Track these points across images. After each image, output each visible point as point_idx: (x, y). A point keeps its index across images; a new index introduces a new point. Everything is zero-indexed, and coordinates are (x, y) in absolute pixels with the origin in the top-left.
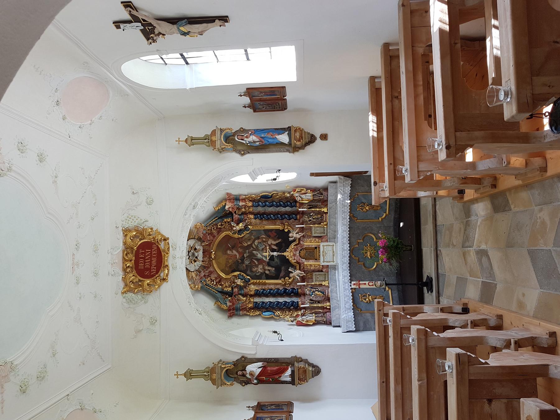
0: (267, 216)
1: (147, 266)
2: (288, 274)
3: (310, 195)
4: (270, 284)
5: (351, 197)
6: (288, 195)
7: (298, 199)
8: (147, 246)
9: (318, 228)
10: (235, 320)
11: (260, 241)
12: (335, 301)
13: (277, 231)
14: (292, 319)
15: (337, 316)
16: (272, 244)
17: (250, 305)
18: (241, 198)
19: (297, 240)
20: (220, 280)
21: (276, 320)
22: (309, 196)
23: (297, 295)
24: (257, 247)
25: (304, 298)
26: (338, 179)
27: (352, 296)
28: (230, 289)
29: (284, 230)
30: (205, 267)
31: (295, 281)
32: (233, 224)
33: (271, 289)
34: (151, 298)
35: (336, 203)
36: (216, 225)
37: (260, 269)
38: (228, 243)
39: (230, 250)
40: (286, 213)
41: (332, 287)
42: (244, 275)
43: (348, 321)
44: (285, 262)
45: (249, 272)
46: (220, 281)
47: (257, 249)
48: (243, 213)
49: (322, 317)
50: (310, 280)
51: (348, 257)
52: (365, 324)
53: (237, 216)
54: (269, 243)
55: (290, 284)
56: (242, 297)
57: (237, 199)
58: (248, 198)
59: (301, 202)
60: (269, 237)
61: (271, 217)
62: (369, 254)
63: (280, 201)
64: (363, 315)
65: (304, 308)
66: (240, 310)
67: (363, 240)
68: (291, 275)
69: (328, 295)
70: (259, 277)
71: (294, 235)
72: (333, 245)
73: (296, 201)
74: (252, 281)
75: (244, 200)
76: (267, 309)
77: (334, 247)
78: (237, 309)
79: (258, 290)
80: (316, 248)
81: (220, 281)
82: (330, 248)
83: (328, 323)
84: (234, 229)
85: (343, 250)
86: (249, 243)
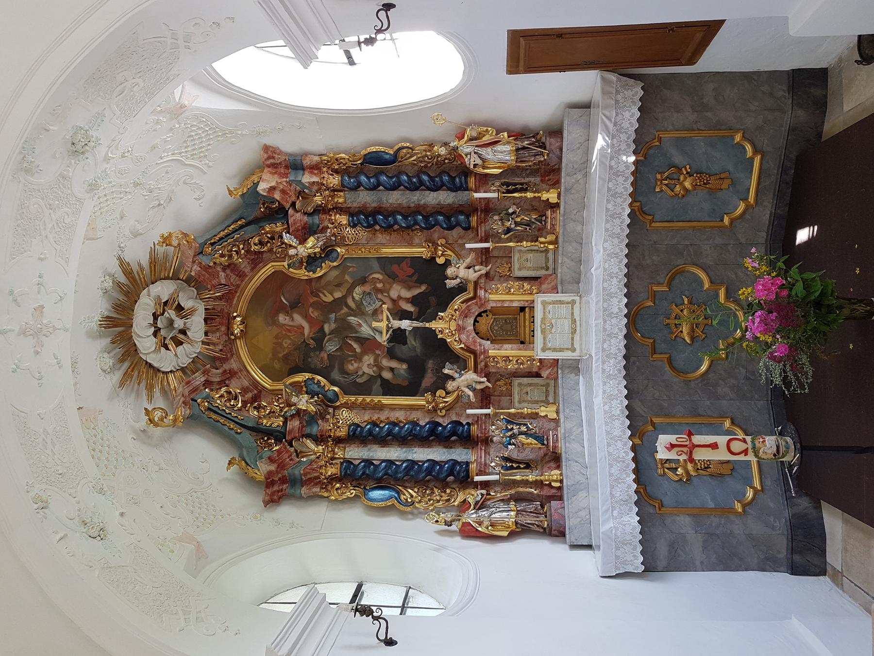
0: (386, 217)
2: (442, 380)
3: (508, 148)
4: (393, 408)
5: (642, 144)
6: (443, 151)
7: (471, 161)
9: (530, 256)
11: (367, 288)
12: (575, 467)
13: (415, 261)
14: (449, 516)
15: (583, 514)
16: (400, 297)
17: (331, 471)
19: (471, 287)
20: (256, 395)
21: (403, 514)
22: (503, 154)
23: (468, 440)
24: (359, 304)
25: (487, 453)
26: (597, 96)
27: (634, 459)
29: (433, 259)
30: (214, 359)
31: (460, 402)
32: (287, 238)
33: (395, 424)
35: (586, 175)
36: (246, 242)
37: (366, 366)
39: (287, 313)
40: (440, 210)
41: (569, 425)
42: (323, 381)
43: (620, 543)
44: (438, 349)
45: (336, 375)
47: (359, 311)
48: (319, 210)
49: (536, 513)
50: (505, 400)
51: (621, 336)
52: (672, 546)
53: (298, 215)
54: (394, 294)
55: (449, 408)
56: (311, 445)
57: (295, 165)
58: (328, 164)
59: (480, 170)
60: (393, 277)
61: (396, 222)
62: (685, 329)
63: (421, 171)
64: (668, 521)
65: (485, 485)
66: (303, 483)
67: (669, 285)
68: (450, 386)
69: (555, 447)
70: (364, 389)
71: (460, 271)
72: (573, 303)
73: (466, 172)
74: (343, 399)
75: (315, 168)
76: (379, 480)
77: (576, 307)
78: (294, 482)
79: (358, 425)
80: (522, 309)
81: (255, 399)
82: (564, 310)
83: (556, 532)
84: (292, 252)
85: (608, 315)
86: (338, 295)
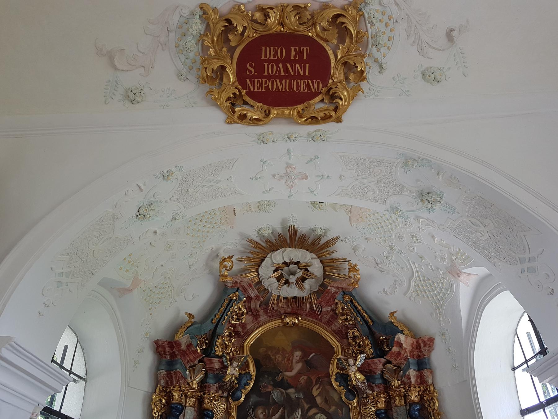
1: (268, 69)
8: (320, 66)
10: (148, 358)
17: (176, 395)
18: (426, 373)
20: (240, 334)
28: (218, 351)
32: (361, 358)
34: (191, 89)
36: (354, 326)
38: (316, 353)
39: (302, 358)
45: (254, 399)
46: (237, 334)
48: (387, 384)
53: (380, 366)
57: (422, 364)
66: (168, 372)
74: (234, 405)
75: (422, 381)
78: (171, 364)
81: (237, 334)
84: (351, 361)
86: (319, 400)
